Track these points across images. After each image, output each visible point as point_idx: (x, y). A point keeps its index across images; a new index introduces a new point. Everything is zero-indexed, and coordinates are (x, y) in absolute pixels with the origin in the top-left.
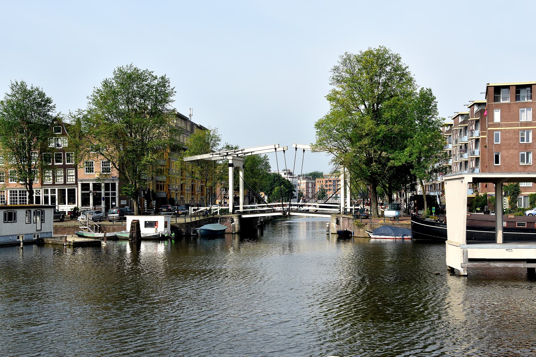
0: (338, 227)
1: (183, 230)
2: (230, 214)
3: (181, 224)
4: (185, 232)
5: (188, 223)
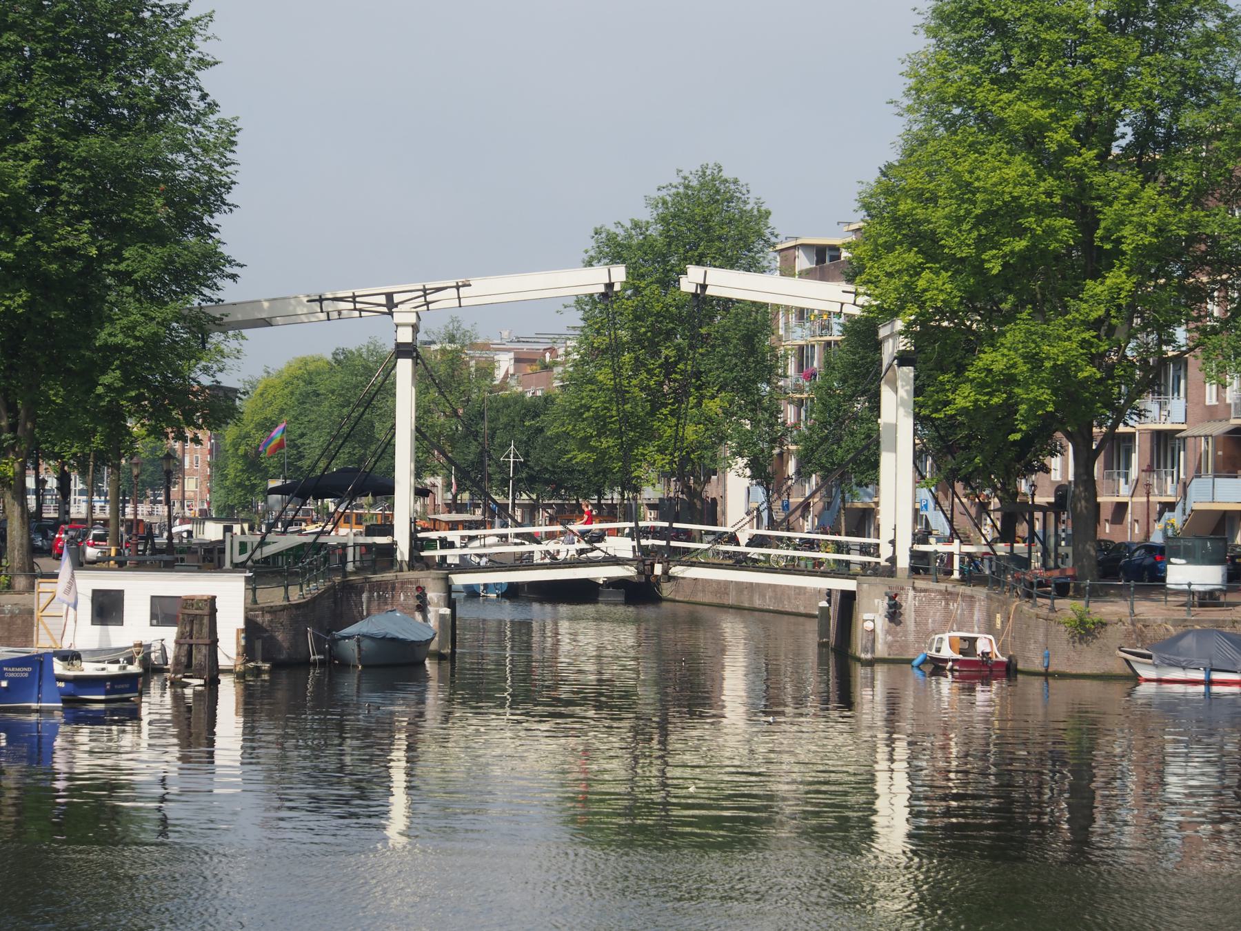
0: (895, 634)
1: (280, 636)
2: (401, 570)
3: (272, 611)
4: (286, 645)
5: (298, 606)
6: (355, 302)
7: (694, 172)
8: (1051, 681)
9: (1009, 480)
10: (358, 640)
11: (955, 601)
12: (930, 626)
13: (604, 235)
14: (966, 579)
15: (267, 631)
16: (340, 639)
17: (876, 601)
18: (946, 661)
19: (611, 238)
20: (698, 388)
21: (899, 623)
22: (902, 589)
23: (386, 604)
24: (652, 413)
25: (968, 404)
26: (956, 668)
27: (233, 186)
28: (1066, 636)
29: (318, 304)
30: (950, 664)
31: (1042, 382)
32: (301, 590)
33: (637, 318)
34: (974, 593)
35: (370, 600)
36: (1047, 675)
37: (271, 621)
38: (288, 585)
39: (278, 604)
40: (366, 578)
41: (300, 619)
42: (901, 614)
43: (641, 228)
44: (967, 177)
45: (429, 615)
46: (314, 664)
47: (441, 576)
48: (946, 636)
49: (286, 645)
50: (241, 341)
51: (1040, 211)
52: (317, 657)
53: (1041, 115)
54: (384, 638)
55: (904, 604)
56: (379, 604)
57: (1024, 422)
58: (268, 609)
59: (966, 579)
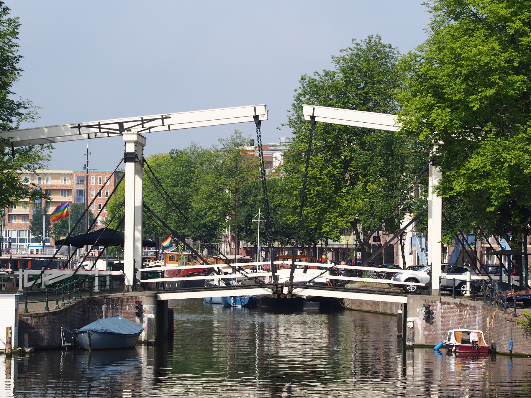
0: (429, 330)
1: (42, 332)
2: (128, 291)
3: (38, 316)
4: (46, 337)
5: (54, 313)
6: (100, 128)
7: (363, 40)
8: (513, 359)
9: (516, 235)
10: (89, 334)
11: (465, 310)
12: (451, 325)
13: (307, 80)
14: (474, 296)
15: (34, 328)
16: (79, 333)
17: (418, 310)
18: (452, 346)
19: (312, 82)
20: (365, 176)
21: (432, 323)
22: (434, 302)
23: (117, 312)
24: (336, 192)
25: (461, 190)
26: (457, 351)
27: (20, 58)
28: (522, 331)
29: (77, 129)
30: (454, 348)
31: (504, 176)
32: (57, 304)
33: (328, 132)
34: (476, 305)
35: (107, 309)
36: (511, 355)
37: (36, 323)
38: (48, 301)
39: (41, 312)
40: (104, 296)
41: (56, 321)
42: (433, 318)
43: (330, 76)
44: (459, 50)
45: (144, 319)
46: (64, 349)
47: (151, 295)
48: (453, 331)
49: (46, 337)
50: (51, 150)
51: (503, 71)
52: (66, 344)
53: (504, 12)
54: (105, 333)
55: (435, 312)
56: (113, 312)
57: (496, 200)
58: (35, 315)
59: (474, 296)
